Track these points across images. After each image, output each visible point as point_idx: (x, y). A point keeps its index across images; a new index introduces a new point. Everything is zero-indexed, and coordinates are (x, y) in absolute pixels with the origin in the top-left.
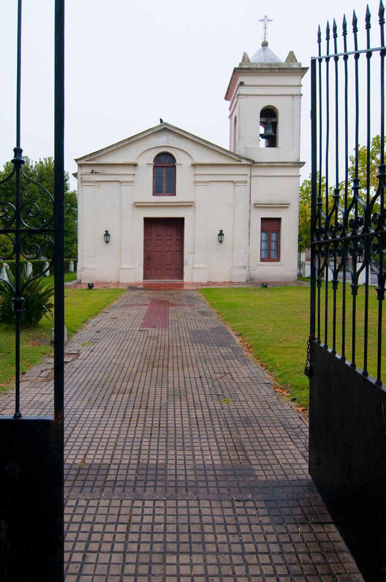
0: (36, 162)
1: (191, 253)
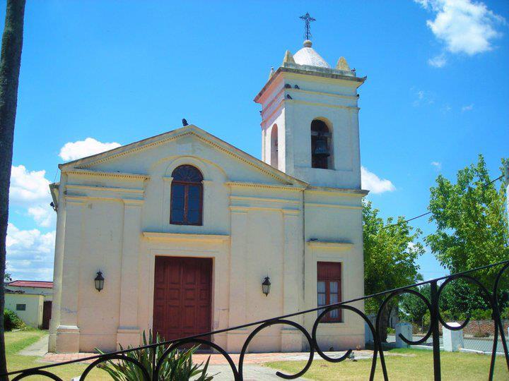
1: (224, 310)
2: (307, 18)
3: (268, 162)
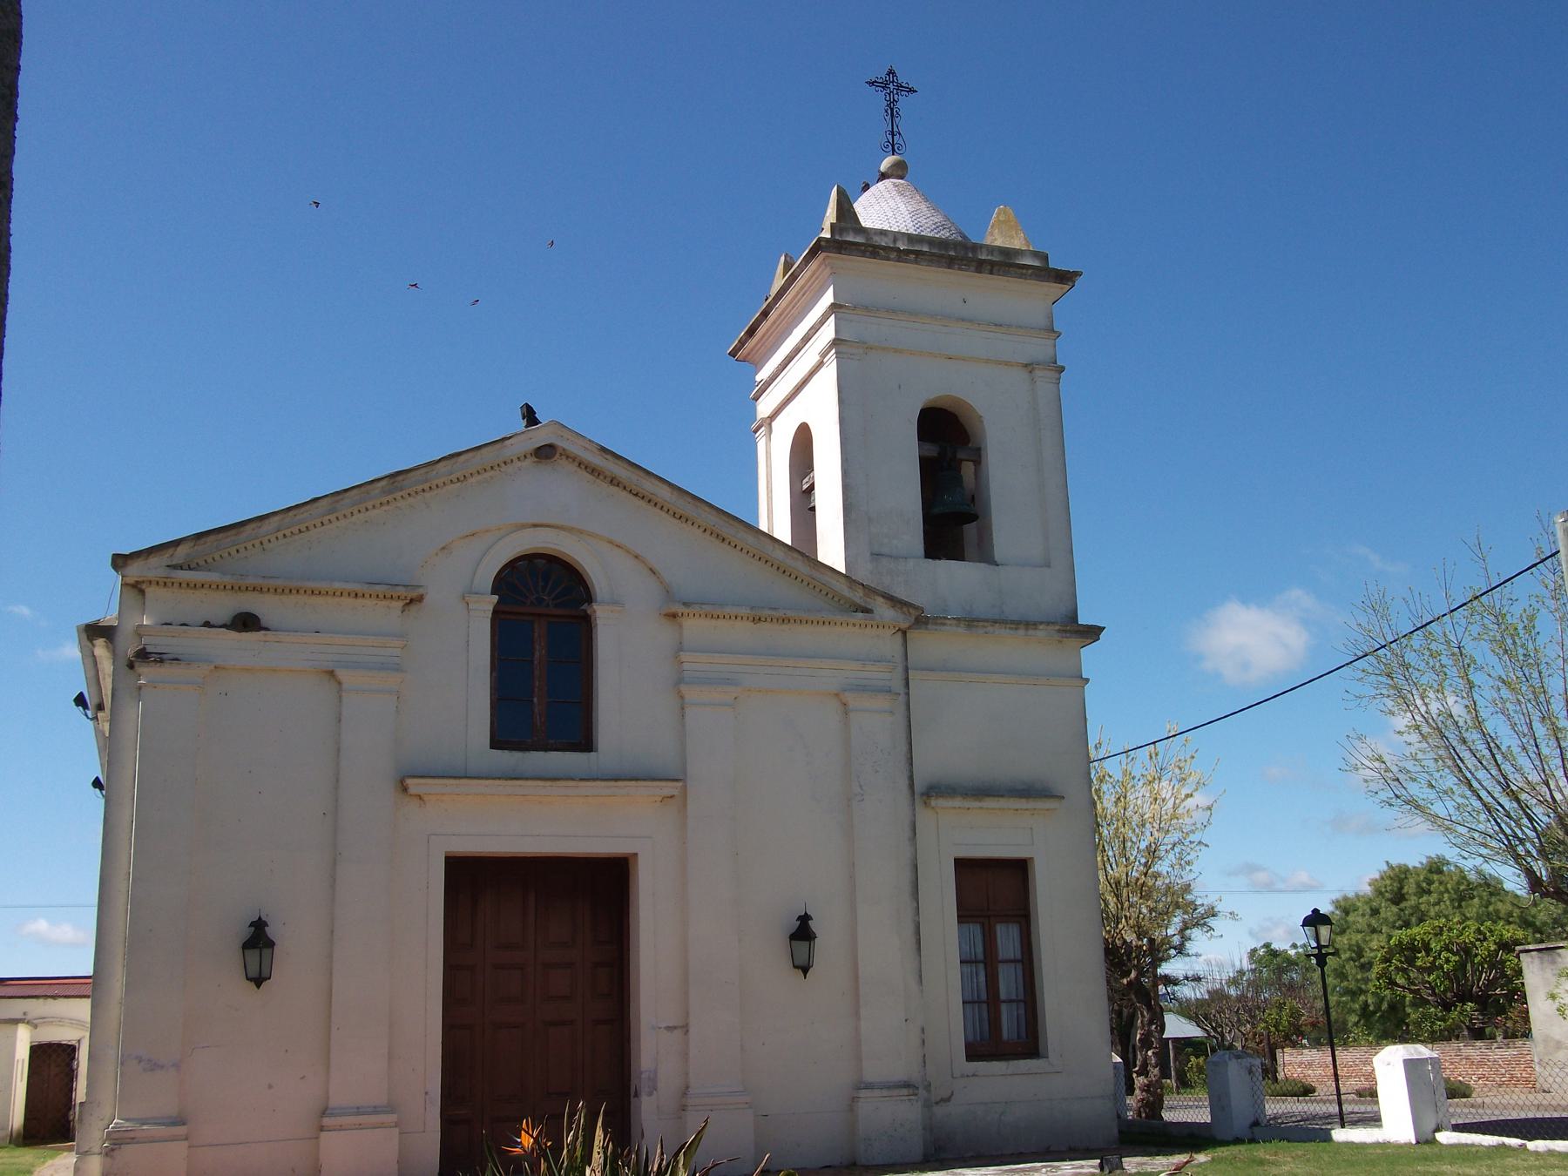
1: (669, 1028)
2: (891, 86)
3: (783, 533)
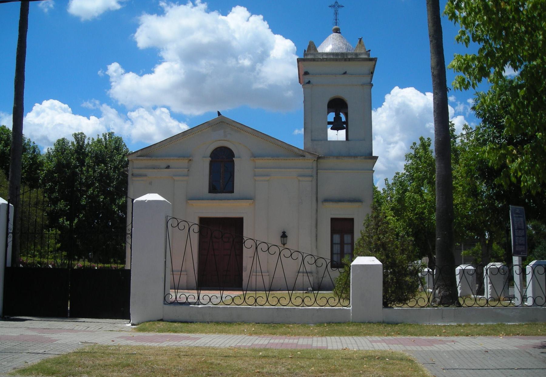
0: (93, 139)
2: (336, 6)
